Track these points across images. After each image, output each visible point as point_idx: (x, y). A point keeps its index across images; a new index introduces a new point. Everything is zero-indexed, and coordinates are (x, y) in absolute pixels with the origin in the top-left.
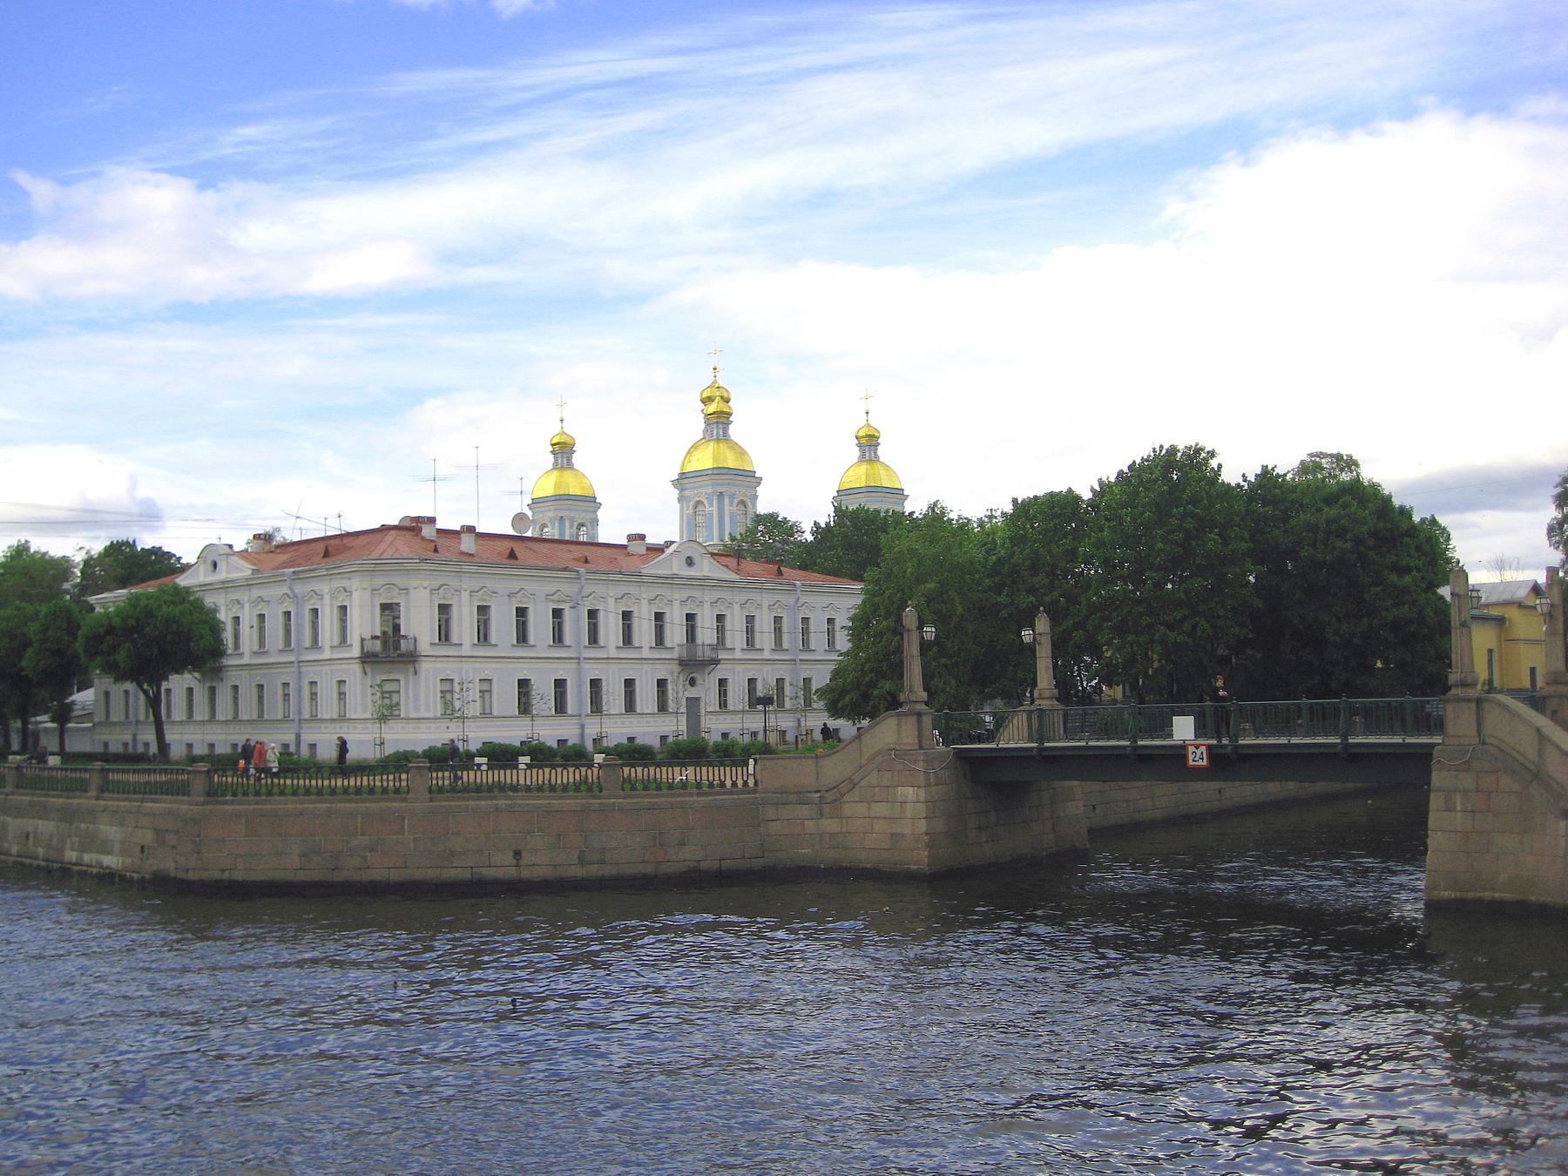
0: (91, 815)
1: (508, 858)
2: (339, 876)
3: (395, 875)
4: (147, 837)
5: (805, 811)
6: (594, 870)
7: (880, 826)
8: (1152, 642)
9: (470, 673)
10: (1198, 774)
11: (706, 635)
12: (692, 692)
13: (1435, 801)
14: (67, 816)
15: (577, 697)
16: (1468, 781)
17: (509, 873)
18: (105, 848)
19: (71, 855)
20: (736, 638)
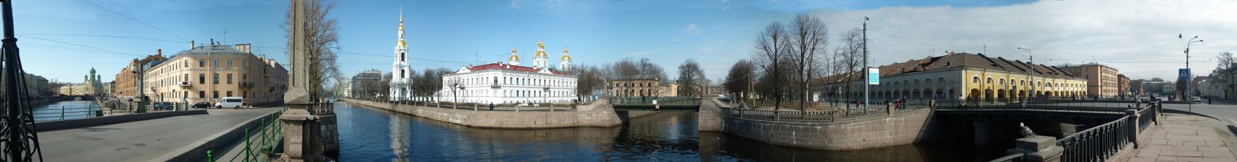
0: (454, 113)
2: (503, 126)
3: (513, 126)
4: (466, 117)
6: (549, 126)
7: (600, 118)
8: (921, 100)
9: (508, 90)
10: (657, 110)
11: (547, 83)
14: (449, 113)
15: (526, 94)
16: (705, 111)
17: (534, 126)
18: (457, 119)
19: (451, 120)
20: (552, 84)
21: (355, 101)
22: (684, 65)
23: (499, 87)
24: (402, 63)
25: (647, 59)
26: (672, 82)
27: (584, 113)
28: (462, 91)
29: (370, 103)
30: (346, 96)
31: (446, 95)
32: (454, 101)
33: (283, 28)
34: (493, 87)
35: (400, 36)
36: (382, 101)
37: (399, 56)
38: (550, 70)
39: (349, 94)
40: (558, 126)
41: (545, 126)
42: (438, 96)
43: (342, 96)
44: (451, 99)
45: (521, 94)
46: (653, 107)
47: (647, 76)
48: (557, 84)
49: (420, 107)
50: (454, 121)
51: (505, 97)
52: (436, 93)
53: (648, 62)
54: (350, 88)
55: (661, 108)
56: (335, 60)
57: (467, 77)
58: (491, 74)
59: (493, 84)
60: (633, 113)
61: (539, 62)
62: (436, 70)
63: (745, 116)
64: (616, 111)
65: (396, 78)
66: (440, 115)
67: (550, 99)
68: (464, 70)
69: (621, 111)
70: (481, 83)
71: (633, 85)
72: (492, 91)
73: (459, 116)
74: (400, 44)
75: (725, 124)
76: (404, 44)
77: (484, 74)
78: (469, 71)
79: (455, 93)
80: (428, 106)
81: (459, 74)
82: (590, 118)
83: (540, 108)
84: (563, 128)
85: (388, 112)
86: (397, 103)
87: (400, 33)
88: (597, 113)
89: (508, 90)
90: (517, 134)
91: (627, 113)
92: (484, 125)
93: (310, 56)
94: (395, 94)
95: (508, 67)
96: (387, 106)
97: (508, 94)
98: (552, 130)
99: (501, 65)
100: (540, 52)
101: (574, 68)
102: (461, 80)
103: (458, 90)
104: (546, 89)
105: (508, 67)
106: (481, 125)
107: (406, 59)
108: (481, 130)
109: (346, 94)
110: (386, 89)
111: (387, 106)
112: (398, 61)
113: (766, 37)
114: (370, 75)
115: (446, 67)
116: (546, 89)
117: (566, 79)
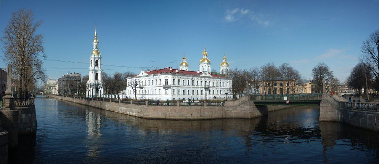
0: (131, 108)
1: (191, 115)
2: (166, 118)
3: (175, 118)
4: (139, 111)
5: (232, 109)
6: (203, 117)
9: (176, 89)
10: (288, 104)
11: (208, 84)
12: (206, 92)
13: (321, 108)
15: (191, 92)
16: (325, 105)
18: (133, 112)
19: (128, 113)
20: (211, 85)
21: (60, 98)
22: (317, 68)
23: (169, 87)
24: (96, 68)
25: (287, 64)
26: (307, 82)
27: (231, 107)
28: (141, 90)
29: (71, 99)
30: (54, 93)
31: (129, 93)
32: (135, 98)
33: (2, 41)
34: (164, 87)
35: (95, 47)
36: (79, 98)
37: (94, 62)
38: (211, 74)
39: (55, 92)
40: (210, 117)
41: (200, 118)
42: (123, 94)
43: (51, 93)
44: (133, 97)
45: (186, 92)
46: (284, 102)
47: (285, 78)
48: (215, 85)
49: (106, 102)
50: (131, 113)
51: (174, 94)
52: (122, 92)
53: (288, 66)
54: (57, 87)
55: (291, 103)
56: (41, 66)
57: (144, 78)
58: (163, 78)
59: (165, 85)
60: (270, 108)
61: (204, 68)
62: (123, 73)
63: (355, 108)
64: (257, 106)
65: (91, 79)
66: (121, 108)
67: (210, 96)
68: (143, 73)
69: (261, 105)
70: (155, 84)
71: (276, 85)
72: (163, 90)
73: (134, 110)
74: (94, 53)
75: (341, 114)
76: (98, 53)
77: (157, 77)
78: (147, 74)
79: (135, 92)
80: (112, 101)
81: (139, 77)
82: (236, 111)
83: (200, 104)
84: (215, 119)
85: (83, 107)
86: (90, 99)
87: (95, 45)
88: (241, 108)
89: (176, 89)
90: (178, 123)
91: (266, 107)
92: (152, 117)
93: (21, 63)
94: (91, 92)
95: (177, 71)
96: (83, 102)
97: (176, 92)
98: (213, 120)
99: (171, 69)
100: (204, 60)
101: (230, 72)
102: (141, 82)
103: (138, 89)
104: (207, 89)
105: (177, 71)
106: (150, 117)
107: (99, 65)
108: (150, 121)
109: (53, 92)
110: (83, 88)
111: (83, 102)
112: (92, 67)
113: (371, 44)
114: (72, 77)
115: (131, 71)
116: (207, 89)
117: (223, 81)
